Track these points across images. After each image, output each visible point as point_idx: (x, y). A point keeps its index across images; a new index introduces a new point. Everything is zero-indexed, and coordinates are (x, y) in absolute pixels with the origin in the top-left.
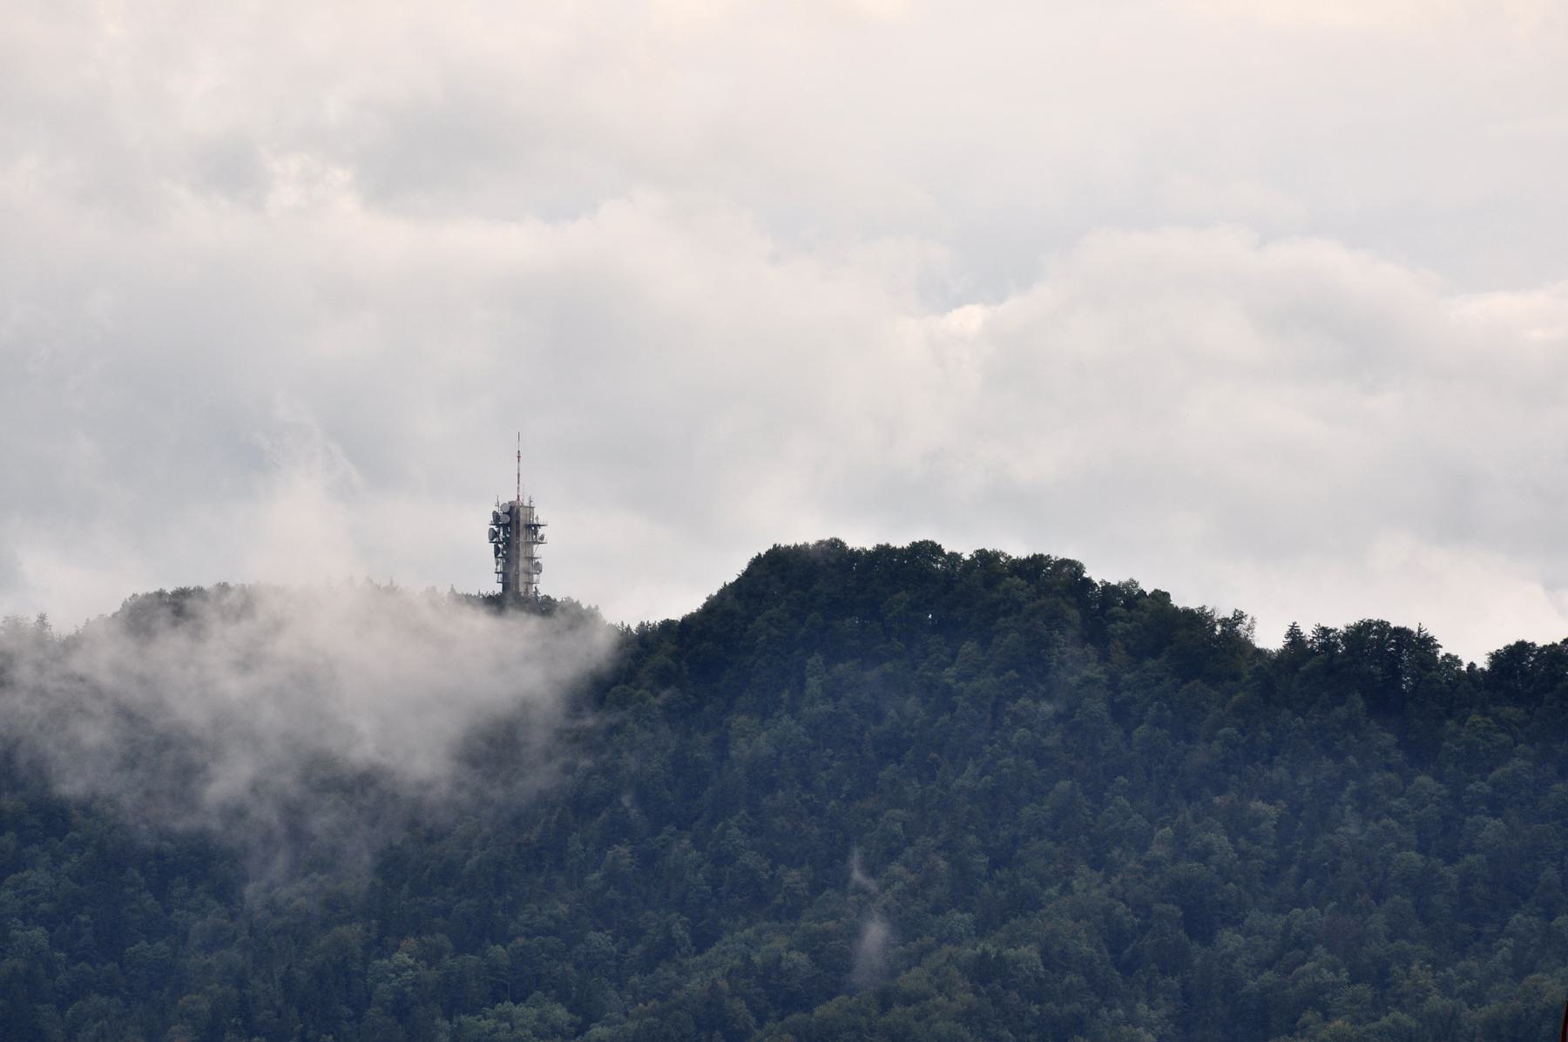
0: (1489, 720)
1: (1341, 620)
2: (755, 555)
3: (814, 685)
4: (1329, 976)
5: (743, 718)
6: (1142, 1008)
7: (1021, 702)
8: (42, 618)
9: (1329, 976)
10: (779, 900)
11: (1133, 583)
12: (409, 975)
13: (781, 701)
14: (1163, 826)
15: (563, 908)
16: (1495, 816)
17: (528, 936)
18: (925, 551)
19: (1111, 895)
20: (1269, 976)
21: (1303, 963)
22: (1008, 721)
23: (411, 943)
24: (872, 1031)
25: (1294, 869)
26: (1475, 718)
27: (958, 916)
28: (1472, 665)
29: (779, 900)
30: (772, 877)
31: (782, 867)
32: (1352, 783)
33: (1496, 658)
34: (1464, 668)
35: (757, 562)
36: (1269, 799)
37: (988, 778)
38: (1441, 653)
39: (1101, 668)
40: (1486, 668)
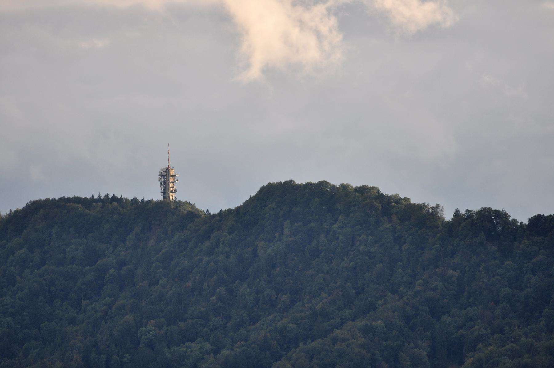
0: (530, 241)
1: (475, 207)
2: (262, 186)
3: (287, 231)
4: (484, 331)
5: (262, 243)
6: (420, 343)
7: (362, 237)
8: (208, 211)
9: (484, 331)
10: (280, 306)
11: (397, 195)
12: (153, 332)
13: (275, 237)
14: (418, 280)
15: (203, 309)
16: (535, 275)
17: (191, 318)
18: (323, 184)
19: (404, 303)
20: (461, 331)
21: (474, 327)
22: (358, 243)
23: (151, 322)
24: (332, 351)
25: (465, 294)
26: (525, 241)
27: (347, 311)
28: (522, 223)
29: (280, 306)
30: (277, 298)
31: (280, 294)
32: (483, 264)
33: (531, 220)
34: (519, 224)
35: (263, 189)
36: (455, 269)
37: (352, 263)
38: (511, 219)
39: (390, 225)
40: (527, 223)
